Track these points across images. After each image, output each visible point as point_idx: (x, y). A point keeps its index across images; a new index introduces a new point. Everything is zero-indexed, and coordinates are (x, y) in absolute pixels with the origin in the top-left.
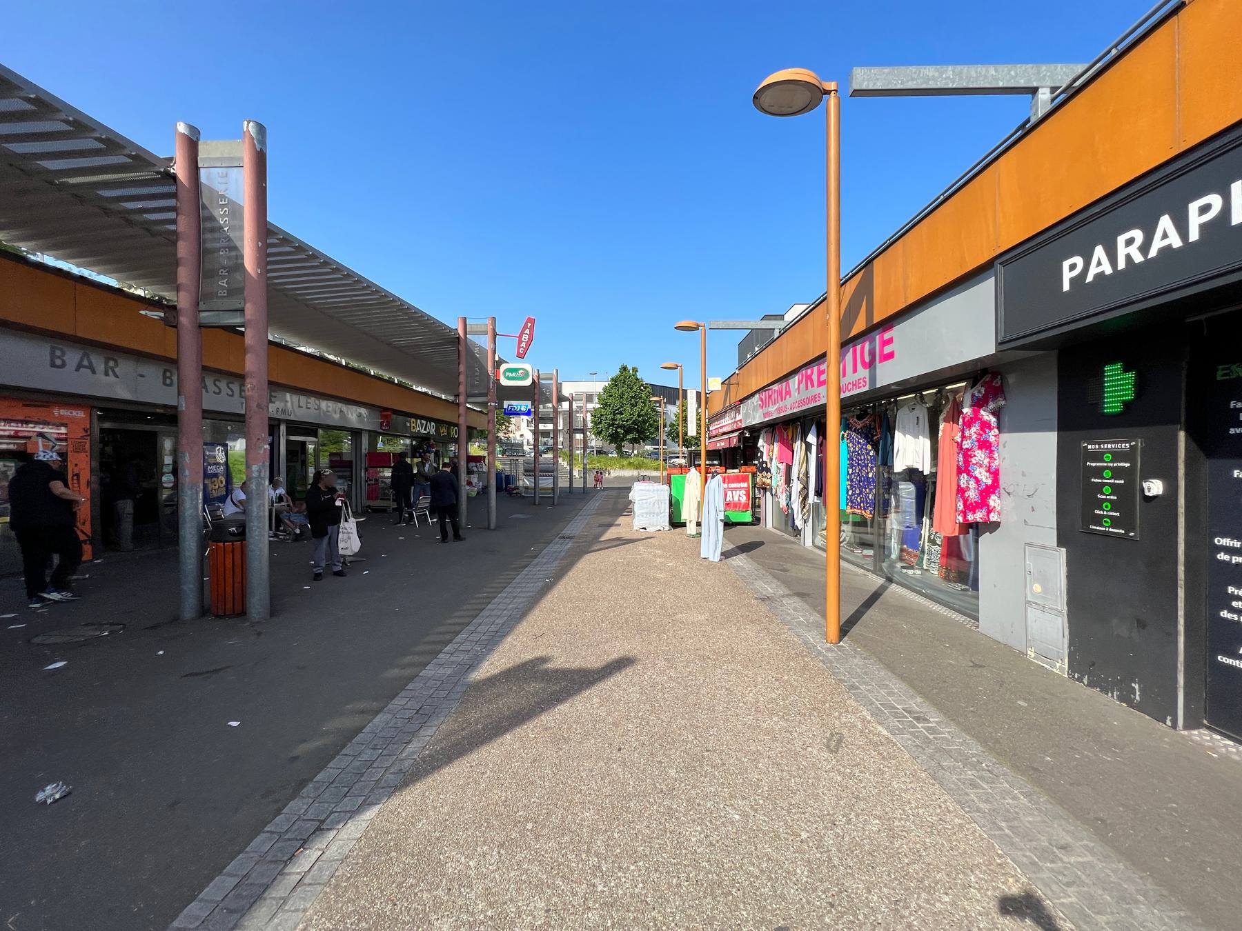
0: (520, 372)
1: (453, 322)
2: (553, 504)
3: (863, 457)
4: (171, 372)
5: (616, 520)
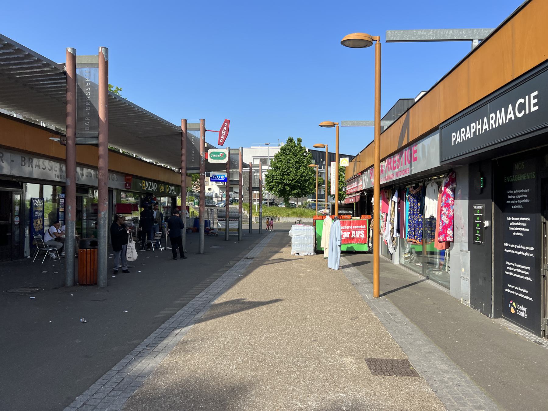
0: (221, 154)
1: (178, 123)
2: (239, 240)
3: (415, 210)
4: (25, 159)
5: (280, 249)
